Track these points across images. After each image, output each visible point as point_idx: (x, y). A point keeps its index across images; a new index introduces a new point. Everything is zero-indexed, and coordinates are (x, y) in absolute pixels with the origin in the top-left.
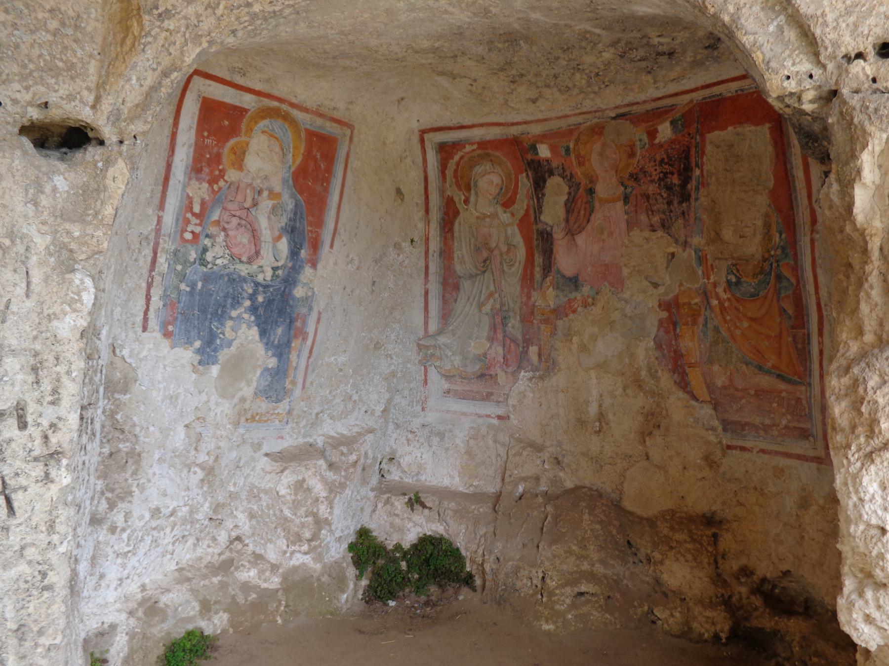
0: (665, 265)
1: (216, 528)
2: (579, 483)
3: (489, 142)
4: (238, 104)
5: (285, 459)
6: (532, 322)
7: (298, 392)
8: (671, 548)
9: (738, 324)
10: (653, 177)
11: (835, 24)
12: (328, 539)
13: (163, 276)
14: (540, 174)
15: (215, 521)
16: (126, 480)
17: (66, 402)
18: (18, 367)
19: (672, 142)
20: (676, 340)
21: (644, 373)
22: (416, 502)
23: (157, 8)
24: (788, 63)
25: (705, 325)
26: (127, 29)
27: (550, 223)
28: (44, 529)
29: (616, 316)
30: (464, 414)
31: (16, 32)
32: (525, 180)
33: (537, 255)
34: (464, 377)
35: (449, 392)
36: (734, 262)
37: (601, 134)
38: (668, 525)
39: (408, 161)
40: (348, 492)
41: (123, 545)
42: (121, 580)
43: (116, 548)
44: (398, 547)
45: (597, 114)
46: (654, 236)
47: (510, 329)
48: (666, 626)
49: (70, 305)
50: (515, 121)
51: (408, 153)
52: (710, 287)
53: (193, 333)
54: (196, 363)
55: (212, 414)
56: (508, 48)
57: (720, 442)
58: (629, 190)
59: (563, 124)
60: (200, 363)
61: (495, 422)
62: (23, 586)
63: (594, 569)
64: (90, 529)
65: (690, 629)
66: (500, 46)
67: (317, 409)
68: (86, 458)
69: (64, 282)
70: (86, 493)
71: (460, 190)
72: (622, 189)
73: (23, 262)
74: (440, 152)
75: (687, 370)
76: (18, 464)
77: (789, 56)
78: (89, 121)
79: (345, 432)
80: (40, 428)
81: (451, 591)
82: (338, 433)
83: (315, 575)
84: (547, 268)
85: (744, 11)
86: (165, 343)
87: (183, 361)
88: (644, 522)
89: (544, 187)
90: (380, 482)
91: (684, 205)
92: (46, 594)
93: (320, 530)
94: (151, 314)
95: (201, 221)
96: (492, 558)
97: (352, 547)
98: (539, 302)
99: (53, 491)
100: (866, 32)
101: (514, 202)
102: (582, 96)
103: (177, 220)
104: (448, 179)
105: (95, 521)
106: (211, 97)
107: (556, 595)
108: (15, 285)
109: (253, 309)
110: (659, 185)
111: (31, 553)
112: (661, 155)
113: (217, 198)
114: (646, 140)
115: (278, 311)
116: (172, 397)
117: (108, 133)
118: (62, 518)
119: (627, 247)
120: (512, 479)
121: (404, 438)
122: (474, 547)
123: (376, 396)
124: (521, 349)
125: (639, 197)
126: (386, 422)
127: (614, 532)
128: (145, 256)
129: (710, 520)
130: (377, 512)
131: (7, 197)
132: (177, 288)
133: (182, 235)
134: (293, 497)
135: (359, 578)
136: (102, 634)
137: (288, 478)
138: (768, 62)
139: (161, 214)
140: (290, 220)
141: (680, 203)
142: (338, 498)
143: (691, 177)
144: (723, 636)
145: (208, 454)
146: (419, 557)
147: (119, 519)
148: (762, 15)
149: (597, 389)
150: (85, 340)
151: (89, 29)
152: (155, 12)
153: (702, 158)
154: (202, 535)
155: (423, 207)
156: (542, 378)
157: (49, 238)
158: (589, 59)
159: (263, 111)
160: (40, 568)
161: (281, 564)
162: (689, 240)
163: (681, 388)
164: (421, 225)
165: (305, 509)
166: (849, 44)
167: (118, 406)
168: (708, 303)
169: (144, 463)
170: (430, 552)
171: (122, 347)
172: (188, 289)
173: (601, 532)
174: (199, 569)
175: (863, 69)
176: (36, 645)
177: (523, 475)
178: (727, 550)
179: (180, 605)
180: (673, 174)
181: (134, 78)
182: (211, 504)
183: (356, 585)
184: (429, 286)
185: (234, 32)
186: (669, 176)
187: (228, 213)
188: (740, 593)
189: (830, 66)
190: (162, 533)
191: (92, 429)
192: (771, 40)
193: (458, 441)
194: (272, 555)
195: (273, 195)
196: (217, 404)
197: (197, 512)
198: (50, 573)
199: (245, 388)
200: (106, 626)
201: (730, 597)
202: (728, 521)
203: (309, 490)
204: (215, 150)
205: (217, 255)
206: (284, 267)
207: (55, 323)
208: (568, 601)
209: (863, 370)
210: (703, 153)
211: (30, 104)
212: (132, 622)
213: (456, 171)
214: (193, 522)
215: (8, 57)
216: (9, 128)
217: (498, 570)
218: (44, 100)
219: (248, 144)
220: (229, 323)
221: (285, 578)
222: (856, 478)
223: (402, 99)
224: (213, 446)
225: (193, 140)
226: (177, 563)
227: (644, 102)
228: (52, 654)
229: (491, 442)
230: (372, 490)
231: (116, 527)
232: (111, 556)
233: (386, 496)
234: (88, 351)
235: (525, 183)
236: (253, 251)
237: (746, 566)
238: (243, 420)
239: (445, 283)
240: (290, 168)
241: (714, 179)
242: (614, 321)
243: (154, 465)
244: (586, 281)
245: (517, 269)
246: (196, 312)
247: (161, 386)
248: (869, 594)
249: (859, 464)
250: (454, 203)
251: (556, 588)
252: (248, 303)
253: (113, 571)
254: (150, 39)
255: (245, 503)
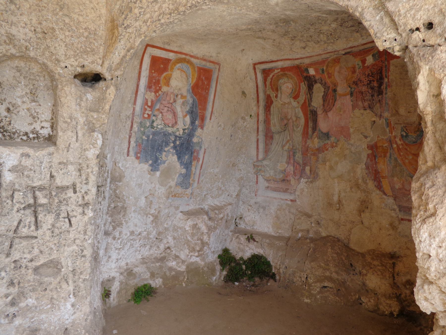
0: (370, 127)
1: (159, 242)
2: (328, 234)
3: (285, 68)
4: (167, 57)
5: (189, 214)
6: (307, 155)
7: (195, 185)
8: (371, 268)
9: (407, 157)
10: (365, 83)
11: (404, 15)
12: (208, 251)
13: (135, 133)
14: (311, 83)
15: (159, 239)
16: (120, 218)
17: (91, 183)
18: (73, 169)
19: (373, 65)
20: (376, 164)
21: (360, 181)
22: (251, 238)
23: (124, 25)
24: (385, 34)
25: (390, 157)
26: (113, 33)
27: (316, 106)
28: (83, 233)
29: (347, 152)
30: (275, 198)
31: (72, 39)
32: (304, 86)
33: (310, 122)
34: (275, 181)
35: (268, 188)
36: (405, 125)
37: (339, 62)
38: (371, 257)
39: (248, 78)
40: (218, 231)
41: (119, 245)
42: (117, 259)
43: (116, 246)
44: (241, 259)
45: (336, 53)
46: (365, 112)
47: (297, 158)
48: (366, 306)
49: (93, 145)
50: (297, 58)
51: (248, 75)
52: (392, 138)
53: (149, 157)
54: (150, 170)
55: (157, 193)
56: (284, 25)
57: (398, 217)
58: (353, 90)
59: (319, 58)
60: (151, 170)
61: (290, 203)
62: (75, 254)
63: (332, 275)
64: (104, 237)
65: (379, 308)
66: (281, 24)
67: (205, 193)
68: (101, 207)
69: (90, 136)
70: (101, 221)
71: (273, 91)
72: (350, 89)
73: (75, 128)
74: (263, 74)
75: (382, 180)
76: (73, 207)
77: (386, 31)
78: (100, 71)
79: (218, 204)
80: (81, 193)
81: (265, 281)
82: (215, 204)
83: (201, 267)
84: (315, 128)
85: (365, 10)
86: (137, 161)
87: (144, 169)
88: (360, 255)
89: (313, 89)
90: (235, 228)
91: (380, 96)
92: (83, 259)
93: (204, 247)
94: (131, 149)
95: (152, 109)
96: (284, 267)
97: (219, 257)
98: (311, 145)
99: (86, 218)
100: (419, 18)
101: (299, 97)
102: (326, 45)
103: (141, 109)
104: (267, 86)
105: (107, 233)
106: (155, 55)
107: (312, 286)
108: (72, 137)
109: (175, 147)
110: (368, 87)
111: (78, 241)
112: (368, 72)
113: (158, 99)
114: (361, 65)
115: (186, 148)
116: (139, 184)
117: (107, 75)
118: (89, 229)
119: (352, 118)
120: (296, 230)
121: (247, 208)
122: (276, 261)
123: (233, 188)
124: (302, 168)
125: (358, 93)
126: (238, 200)
127: (344, 259)
128: (128, 125)
129: (393, 256)
130: (233, 242)
131: (69, 103)
132: (142, 138)
133: (143, 116)
134: (192, 231)
135: (222, 270)
136: (109, 280)
137: (190, 223)
138: (376, 34)
139: (134, 106)
140: (191, 107)
141: (378, 95)
142: (212, 233)
143: (383, 83)
144: (395, 313)
145: (155, 210)
146: (251, 264)
147: (117, 234)
148: (373, 12)
149: (338, 188)
150: (98, 159)
151: (100, 34)
152: (123, 26)
153: (388, 73)
154: (153, 245)
155: (256, 99)
156: (311, 182)
157: (85, 118)
158: (325, 28)
159: (178, 60)
160: (81, 248)
161: (186, 260)
162: (382, 114)
163: (378, 188)
164: (255, 108)
165: (197, 237)
166: (411, 24)
167: (117, 187)
168: (392, 146)
169: (127, 212)
170: (256, 262)
171: (119, 162)
172: (146, 138)
173: (337, 258)
174: (151, 259)
175: (418, 35)
176: (79, 278)
177: (302, 228)
178: (400, 271)
179: (142, 273)
180: (374, 81)
181: (117, 53)
182: (156, 231)
183: (220, 273)
184: (259, 137)
185: (155, 31)
186: (372, 82)
187: (163, 105)
188: (406, 293)
189: (404, 35)
190: (135, 242)
191: (104, 196)
192: (377, 24)
193: (272, 211)
194: (183, 257)
195: (183, 97)
196: (159, 188)
197: (151, 234)
198: (85, 251)
199: (171, 182)
200: (111, 277)
201: (400, 295)
202: (402, 257)
203: (199, 229)
204: (157, 78)
205: (158, 124)
206: (188, 128)
207: (87, 152)
208: (318, 290)
209: (425, 180)
210: (389, 70)
211: (77, 66)
212: (122, 277)
213: (271, 82)
214: (149, 239)
215: (69, 48)
216: (70, 76)
217: (286, 272)
218: (82, 64)
219: (171, 75)
220: (164, 153)
221: (188, 267)
222: (419, 229)
223: (243, 50)
224: (157, 207)
225: (148, 75)
226: (142, 256)
227: (358, 46)
228: (85, 283)
229: (287, 212)
230: (231, 231)
231: (116, 237)
232: (114, 249)
233: (237, 235)
234: (101, 164)
235: (304, 87)
236: (174, 122)
237: (409, 280)
238: (171, 196)
239: (266, 136)
240: (190, 84)
241: (394, 83)
242: (346, 155)
243: (132, 213)
244: (332, 135)
245: (300, 129)
246: (150, 148)
247: (135, 180)
248: (426, 287)
249: (420, 224)
250: (271, 97)
251: (312, 283)
252: (172, 145)
253: (114, 255)
254: (122, 37)
255: (172, 233)
